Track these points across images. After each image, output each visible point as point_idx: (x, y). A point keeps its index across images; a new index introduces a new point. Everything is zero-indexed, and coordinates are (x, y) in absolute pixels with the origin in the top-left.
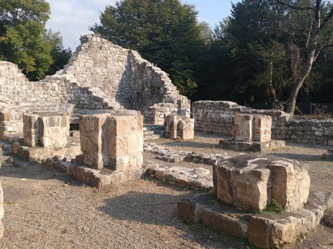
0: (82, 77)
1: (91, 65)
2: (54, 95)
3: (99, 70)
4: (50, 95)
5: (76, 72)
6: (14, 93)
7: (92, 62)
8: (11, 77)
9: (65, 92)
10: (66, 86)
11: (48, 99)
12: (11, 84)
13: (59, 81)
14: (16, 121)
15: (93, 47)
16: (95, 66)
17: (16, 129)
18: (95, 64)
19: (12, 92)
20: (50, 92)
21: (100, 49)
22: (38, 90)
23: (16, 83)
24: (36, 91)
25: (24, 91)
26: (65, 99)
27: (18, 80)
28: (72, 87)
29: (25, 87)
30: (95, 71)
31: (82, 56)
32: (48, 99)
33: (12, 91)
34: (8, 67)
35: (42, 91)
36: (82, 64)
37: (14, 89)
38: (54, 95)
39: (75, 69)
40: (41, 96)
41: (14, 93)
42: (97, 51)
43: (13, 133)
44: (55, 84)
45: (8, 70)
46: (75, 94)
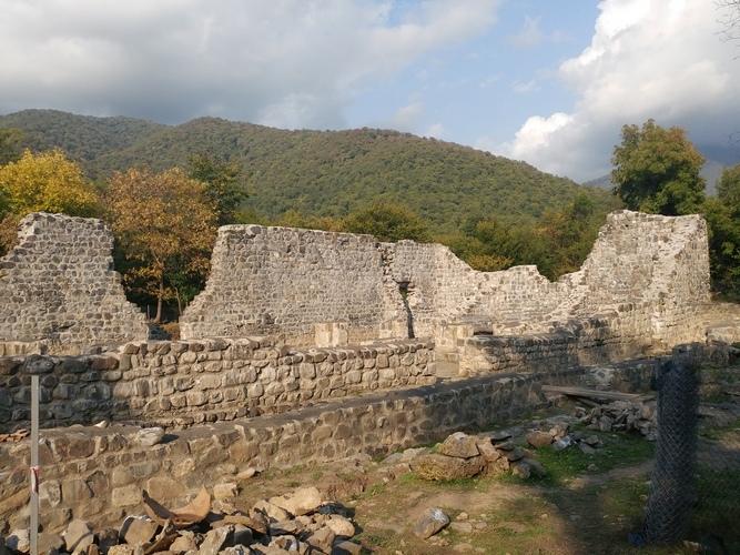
3: (625, 258)
16: (618, 254)
36: (599, 255)
37: (524, 293)
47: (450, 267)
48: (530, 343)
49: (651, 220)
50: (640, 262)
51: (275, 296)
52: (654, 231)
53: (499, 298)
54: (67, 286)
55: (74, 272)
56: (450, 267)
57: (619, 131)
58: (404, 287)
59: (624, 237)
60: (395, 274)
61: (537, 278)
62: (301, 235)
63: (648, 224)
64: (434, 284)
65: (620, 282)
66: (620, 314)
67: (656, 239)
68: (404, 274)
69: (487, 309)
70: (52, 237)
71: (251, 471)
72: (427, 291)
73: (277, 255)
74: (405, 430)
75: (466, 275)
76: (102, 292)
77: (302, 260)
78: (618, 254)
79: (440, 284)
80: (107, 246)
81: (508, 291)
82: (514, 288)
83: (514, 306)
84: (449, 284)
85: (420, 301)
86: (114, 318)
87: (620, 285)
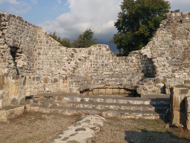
0: (160, 50)
1: (170, 39)
2: (132, 66)
3: (178, 42)
4: (130, 66)
5: (154, 46)
6: (102, 65)
7: (171, 36)
8: (101, 54)
9: (140, 63)
10: (140, 58)
11: (128, 70)
12: (101, 59)
13: (136, 55)
14: (51, 84)
15: (172, 22)
16: (173, 39)
17: (51, 90)
18: (174, 38)
19: (101, 65)
20: (130, 64)
21: (181, 23)
22: (122, 62)
23: (104, 58)
24: (120, 63)
25: (111, 64)
26: (140, 69)
27: (106, 56)
28: (144, 59)
29: (111, 61)
30: (173, 43)
31: (160, 31)
32: (128, 70)
33: (101, 64)
34: (99, 47)
35: (124, 63)
36: (160, 39)
37: (103, 62)
38: (132, 66)
39: (154, 43)
40: (124, 67)
41: (102, 65)
42: (176, 25)
43: (49, 92)
44: (133, 58)
45: (99, 50)
46: (146, 65)
47: (47, 42)
48: (23, 113)
53: (88, 64)
56: (47, 42)
57: (80, 34)
58: (14, 51)
59: (178, 28)
60: (7, 39)
64: (35, 53)
65: (174, 58)
68: (14, 41)
69: (81, 72)
72: (30, 57)
75: (59, 49)
78: (173, 39)
79: (39, 54)
81: (93, 60)
82: (96, 58)
83: (97, 70)
84: (46, 54)
85: (26, 64)
87: (174, 60)
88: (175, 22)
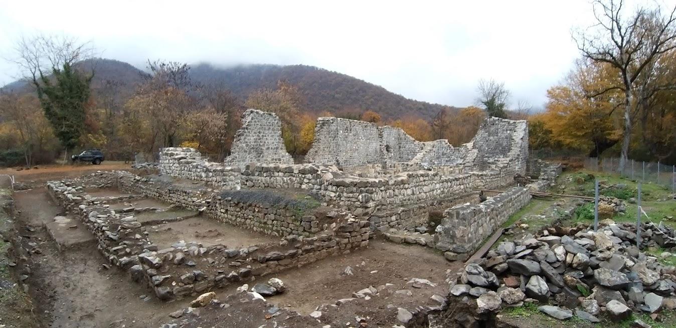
3: (491, 138)
15: (488, 125)
36: (480, 136)
47: (405, 139)
49: (504, 122)
50: (499, 140)
51: (340, 151)
52: (506, 127)
54: (264, 145)
55: (267, 139)
61: (449, 146)
62: (350, 123)
63: (504, 123)
66: (510, 163)
67: (507, 130)
70: (258, 121)
71: (145, 180)
73: (341, 132)
74: (635, 232)
76: (277, 148)
77: (350, 134)
78: (489, 136)
80: (279, 126)
84: (405, 147)
86: (282, 161)
88: (489, 124)
